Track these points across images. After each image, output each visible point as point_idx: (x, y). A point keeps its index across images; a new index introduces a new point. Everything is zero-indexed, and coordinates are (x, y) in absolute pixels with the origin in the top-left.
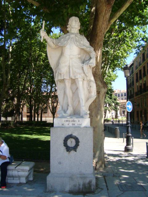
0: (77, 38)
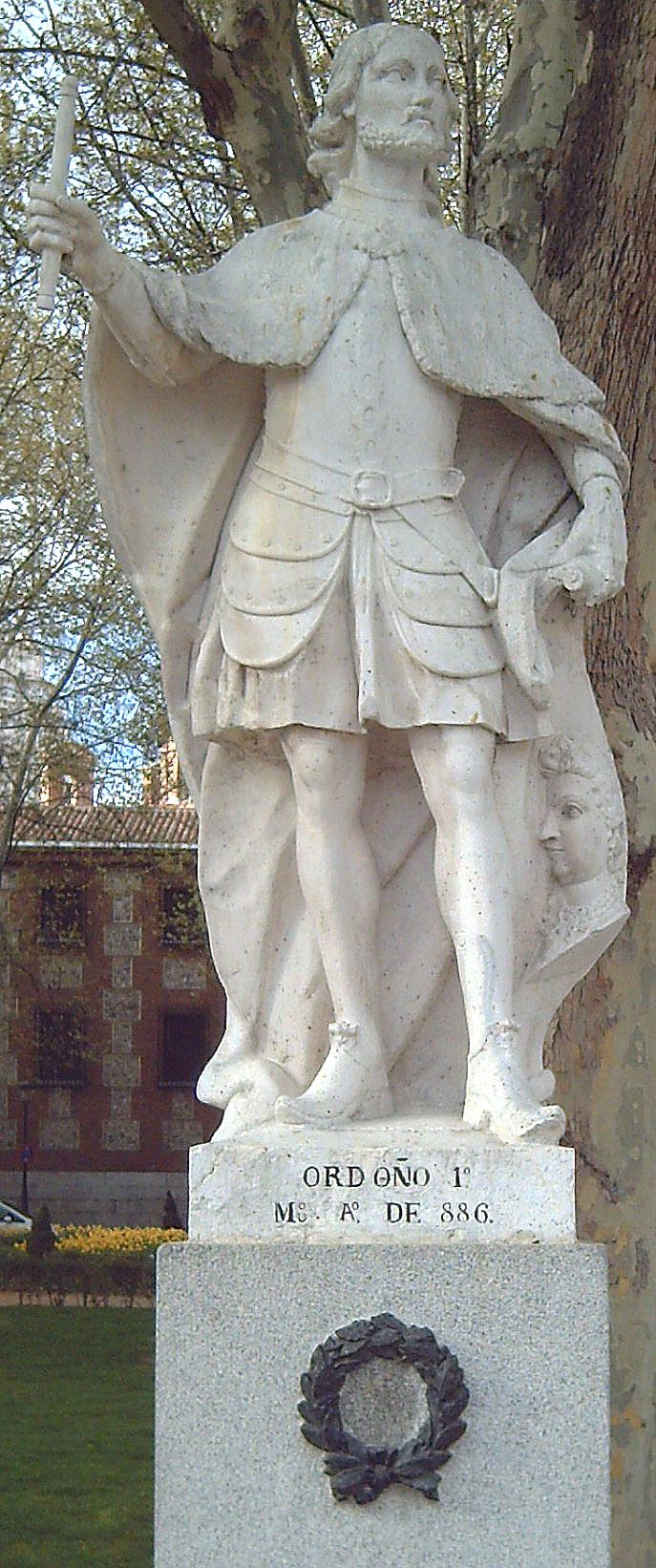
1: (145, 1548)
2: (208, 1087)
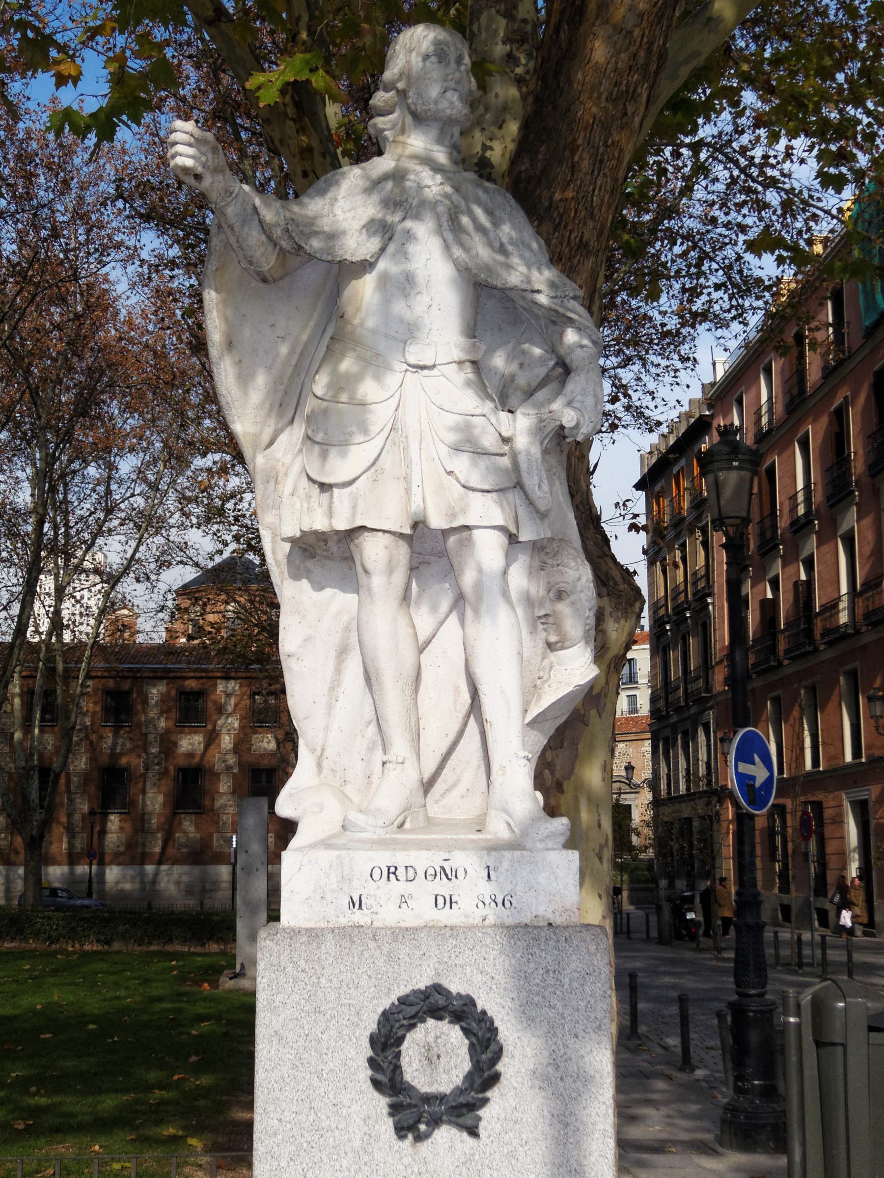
0: (589, 177)
1: (236, 1140)
2: (284, 807)
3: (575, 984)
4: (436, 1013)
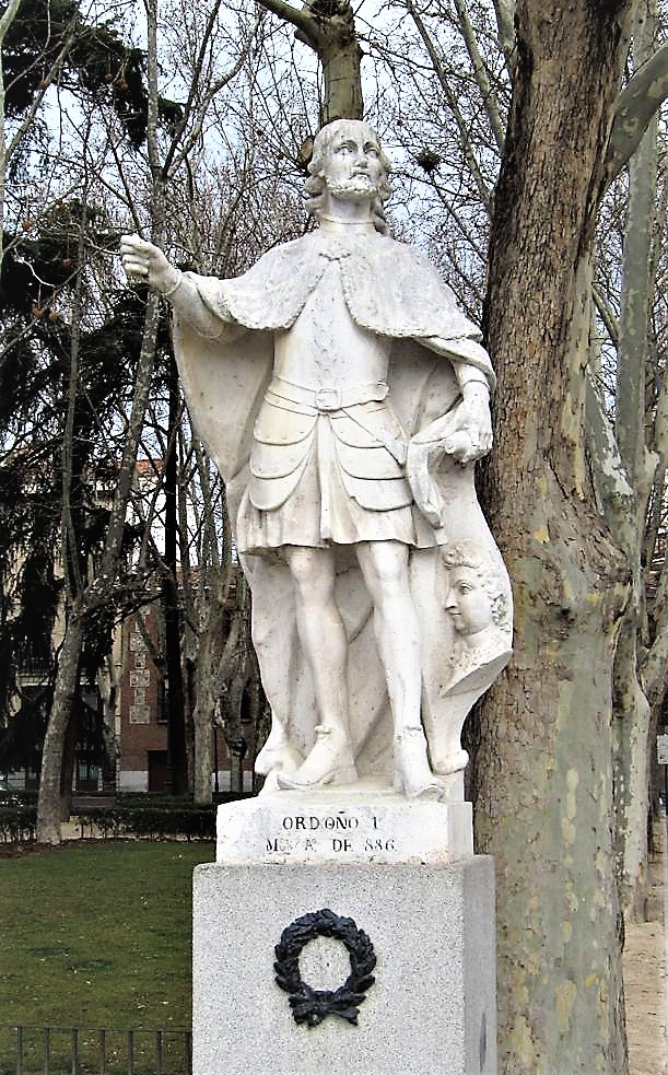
3: (435, 911)
4: (339, 936)
